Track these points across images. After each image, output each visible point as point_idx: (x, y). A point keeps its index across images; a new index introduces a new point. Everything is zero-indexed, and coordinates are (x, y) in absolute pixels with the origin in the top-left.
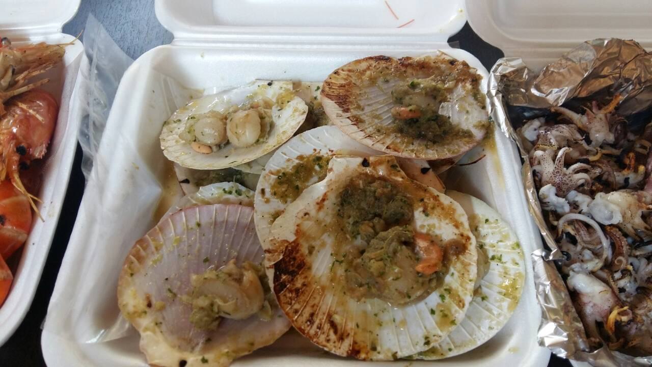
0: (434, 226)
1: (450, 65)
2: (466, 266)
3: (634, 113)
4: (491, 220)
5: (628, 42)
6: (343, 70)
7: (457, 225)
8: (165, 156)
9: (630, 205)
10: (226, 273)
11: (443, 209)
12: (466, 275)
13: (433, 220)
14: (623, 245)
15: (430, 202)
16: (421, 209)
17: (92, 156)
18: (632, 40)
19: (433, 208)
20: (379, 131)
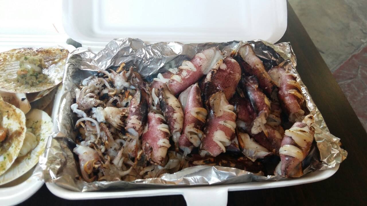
0: (10, 124)
1: (61, 52)
2: (19, 142)
3: (150, 74)
4: (47, 122)
5: (136, 40)
6: (4, 53)
7: (20, 123)
8: (31, 106)
9: (112, 112)
10: (67, 154)
11: (16, 116)
12: (18, 147)
13: (11, 121)
14: (107, 131)
15: (11, 113)
16: (6, 116)
17: (151, 119)
18: (138, 39)
19: (12, 115)
20: (6, 81)
